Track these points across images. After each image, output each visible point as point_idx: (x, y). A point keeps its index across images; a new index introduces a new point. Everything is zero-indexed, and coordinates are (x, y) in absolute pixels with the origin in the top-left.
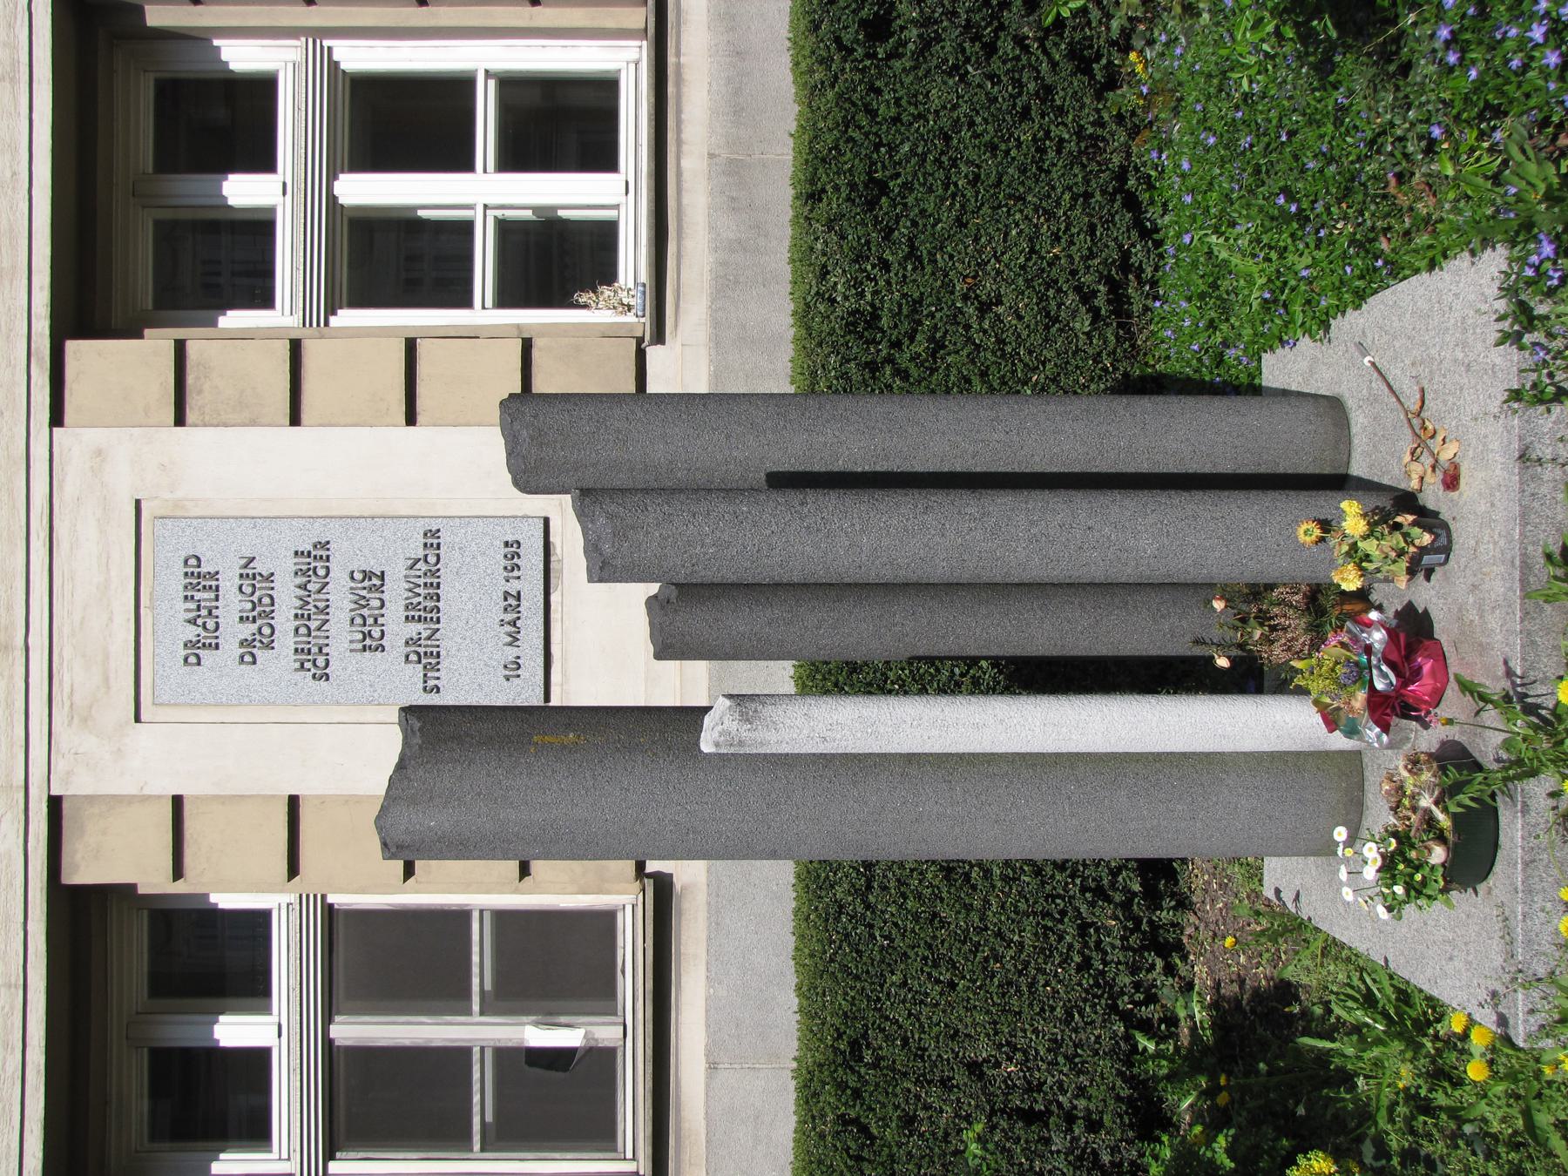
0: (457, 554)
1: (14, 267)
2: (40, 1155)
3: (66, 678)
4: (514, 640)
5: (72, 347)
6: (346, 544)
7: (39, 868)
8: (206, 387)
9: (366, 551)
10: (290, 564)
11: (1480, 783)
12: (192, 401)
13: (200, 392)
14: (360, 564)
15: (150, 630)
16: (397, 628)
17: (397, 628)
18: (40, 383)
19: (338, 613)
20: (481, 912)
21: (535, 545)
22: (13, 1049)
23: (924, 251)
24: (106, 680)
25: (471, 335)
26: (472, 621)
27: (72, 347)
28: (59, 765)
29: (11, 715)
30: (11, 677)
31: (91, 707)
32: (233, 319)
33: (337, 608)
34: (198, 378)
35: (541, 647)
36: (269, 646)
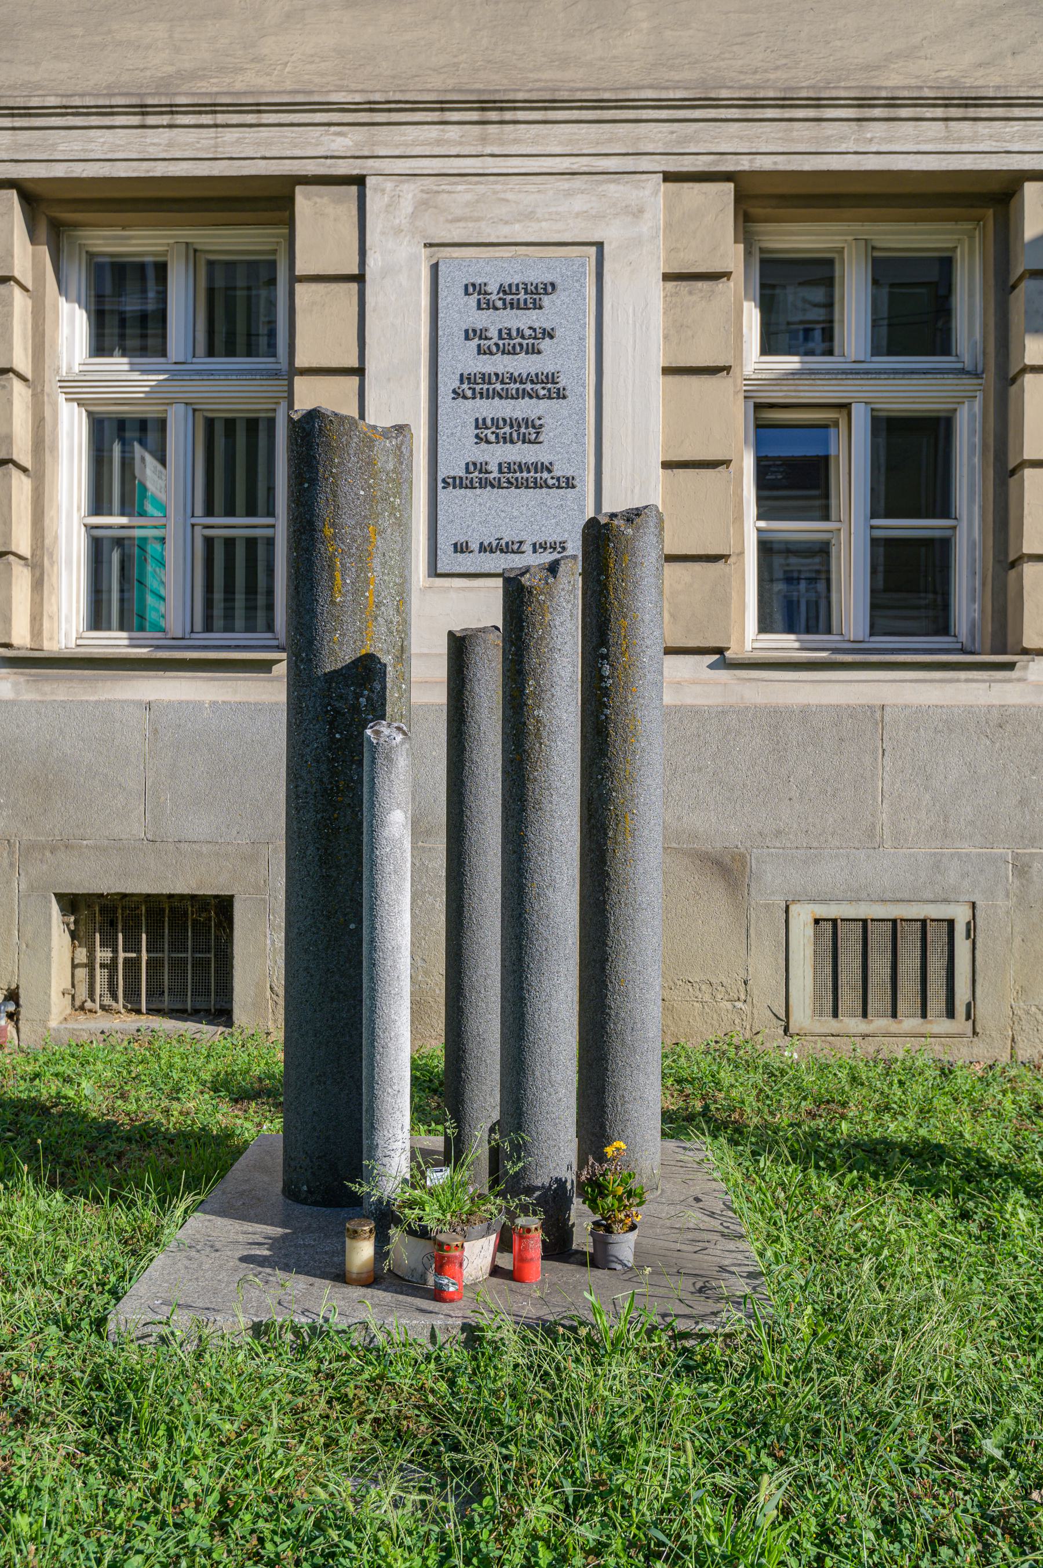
0: (558, 503)
1: (793, 140)
2: (84, 175)
3: (460, 188)
4: (482, 548)
5: (728, 188)
6: (566, 413)
7: (308, 168)
8: (694, 298)
9: (560, 430)
10: (550, 368)
11: (308, 1370)
12: (684, 286)
13: (690, 293)
14: (547, 421)
15: (497, 255)
16: (496, 455)
17: (496, 455)
18: (699, 163)
19: (511, 407)
20: (273, 526)
21: (378, 256)
22: (166, 151)
23: (967, 1487)
24: (458, 220)
25: (739, 518)
26: (503, 515)
27: (728, 188)
28: (389, 184)
29: (430, 144)
30: (461, 144)
31: (436, 207)
32: (752, 317)
33: (514, 406)
34: (701, 291)
35: (483, 571)
36: (480, 351)
